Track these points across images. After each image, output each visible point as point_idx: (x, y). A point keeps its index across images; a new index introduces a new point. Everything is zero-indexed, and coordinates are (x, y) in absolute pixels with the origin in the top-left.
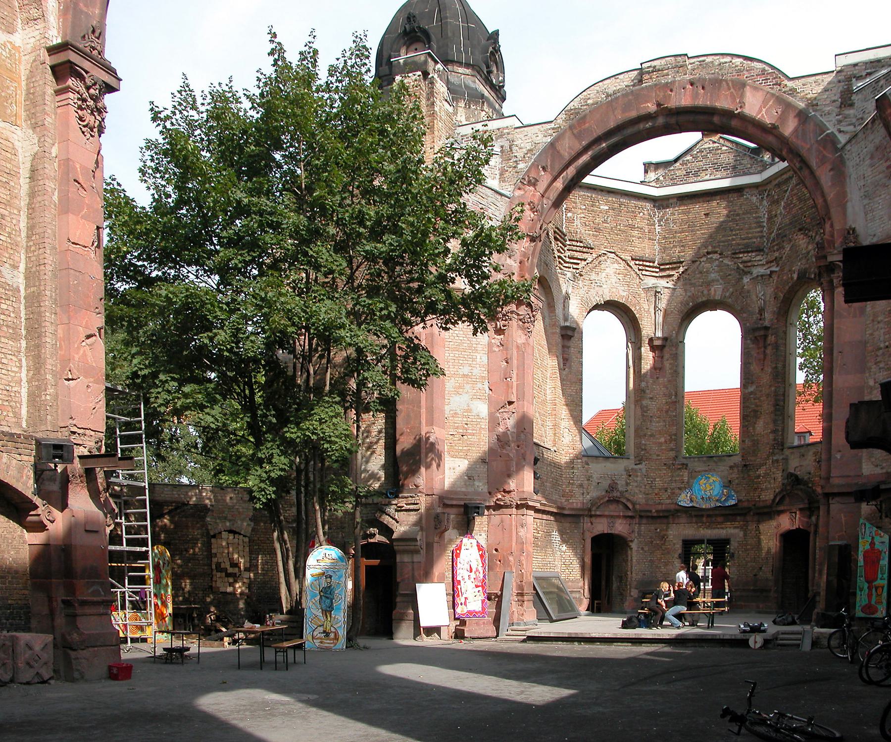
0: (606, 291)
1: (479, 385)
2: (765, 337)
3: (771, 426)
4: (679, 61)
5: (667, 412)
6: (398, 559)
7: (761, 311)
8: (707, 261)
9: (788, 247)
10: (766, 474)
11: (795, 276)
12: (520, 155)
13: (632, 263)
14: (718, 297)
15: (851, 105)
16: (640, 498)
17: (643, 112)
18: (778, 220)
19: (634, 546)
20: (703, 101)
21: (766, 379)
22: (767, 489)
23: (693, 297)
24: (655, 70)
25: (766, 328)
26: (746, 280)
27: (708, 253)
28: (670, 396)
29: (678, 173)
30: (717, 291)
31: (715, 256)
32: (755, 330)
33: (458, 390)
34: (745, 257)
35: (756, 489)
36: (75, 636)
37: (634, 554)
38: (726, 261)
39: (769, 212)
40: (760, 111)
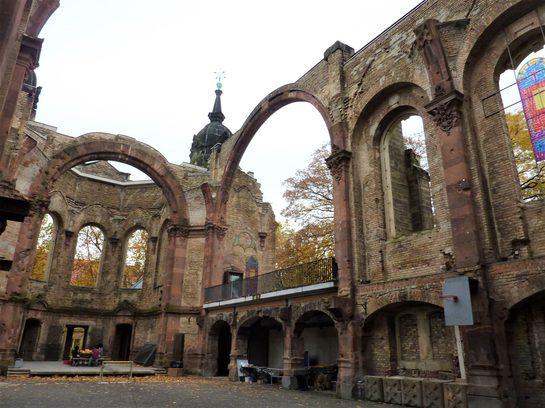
0: (54, 207)
1: (14, 238)
2: (116, 243)
3: (115, 279)
5: (68, 264)
7: (116, 232)
8: (96, 207)
9: (132, 212)
10: (110, 299)
11: (135, 224)
12: (57, 144)
13: (66, 198)
14: (98, 222)
15: (187, 179)
16: (49, 302)
18: (129, 201)
20: (139, 157)
22: (109, 305)
24: (123, 139)
25: (118, 240)
26: (111, 219)
27: (97, 204)
29: (89, 170)
30: (98, 220)
31: (100, 206)
32: (112, 239)
34: (112, 210)
35: (104, 304)
38: (104, 209)
39: (124, 197)
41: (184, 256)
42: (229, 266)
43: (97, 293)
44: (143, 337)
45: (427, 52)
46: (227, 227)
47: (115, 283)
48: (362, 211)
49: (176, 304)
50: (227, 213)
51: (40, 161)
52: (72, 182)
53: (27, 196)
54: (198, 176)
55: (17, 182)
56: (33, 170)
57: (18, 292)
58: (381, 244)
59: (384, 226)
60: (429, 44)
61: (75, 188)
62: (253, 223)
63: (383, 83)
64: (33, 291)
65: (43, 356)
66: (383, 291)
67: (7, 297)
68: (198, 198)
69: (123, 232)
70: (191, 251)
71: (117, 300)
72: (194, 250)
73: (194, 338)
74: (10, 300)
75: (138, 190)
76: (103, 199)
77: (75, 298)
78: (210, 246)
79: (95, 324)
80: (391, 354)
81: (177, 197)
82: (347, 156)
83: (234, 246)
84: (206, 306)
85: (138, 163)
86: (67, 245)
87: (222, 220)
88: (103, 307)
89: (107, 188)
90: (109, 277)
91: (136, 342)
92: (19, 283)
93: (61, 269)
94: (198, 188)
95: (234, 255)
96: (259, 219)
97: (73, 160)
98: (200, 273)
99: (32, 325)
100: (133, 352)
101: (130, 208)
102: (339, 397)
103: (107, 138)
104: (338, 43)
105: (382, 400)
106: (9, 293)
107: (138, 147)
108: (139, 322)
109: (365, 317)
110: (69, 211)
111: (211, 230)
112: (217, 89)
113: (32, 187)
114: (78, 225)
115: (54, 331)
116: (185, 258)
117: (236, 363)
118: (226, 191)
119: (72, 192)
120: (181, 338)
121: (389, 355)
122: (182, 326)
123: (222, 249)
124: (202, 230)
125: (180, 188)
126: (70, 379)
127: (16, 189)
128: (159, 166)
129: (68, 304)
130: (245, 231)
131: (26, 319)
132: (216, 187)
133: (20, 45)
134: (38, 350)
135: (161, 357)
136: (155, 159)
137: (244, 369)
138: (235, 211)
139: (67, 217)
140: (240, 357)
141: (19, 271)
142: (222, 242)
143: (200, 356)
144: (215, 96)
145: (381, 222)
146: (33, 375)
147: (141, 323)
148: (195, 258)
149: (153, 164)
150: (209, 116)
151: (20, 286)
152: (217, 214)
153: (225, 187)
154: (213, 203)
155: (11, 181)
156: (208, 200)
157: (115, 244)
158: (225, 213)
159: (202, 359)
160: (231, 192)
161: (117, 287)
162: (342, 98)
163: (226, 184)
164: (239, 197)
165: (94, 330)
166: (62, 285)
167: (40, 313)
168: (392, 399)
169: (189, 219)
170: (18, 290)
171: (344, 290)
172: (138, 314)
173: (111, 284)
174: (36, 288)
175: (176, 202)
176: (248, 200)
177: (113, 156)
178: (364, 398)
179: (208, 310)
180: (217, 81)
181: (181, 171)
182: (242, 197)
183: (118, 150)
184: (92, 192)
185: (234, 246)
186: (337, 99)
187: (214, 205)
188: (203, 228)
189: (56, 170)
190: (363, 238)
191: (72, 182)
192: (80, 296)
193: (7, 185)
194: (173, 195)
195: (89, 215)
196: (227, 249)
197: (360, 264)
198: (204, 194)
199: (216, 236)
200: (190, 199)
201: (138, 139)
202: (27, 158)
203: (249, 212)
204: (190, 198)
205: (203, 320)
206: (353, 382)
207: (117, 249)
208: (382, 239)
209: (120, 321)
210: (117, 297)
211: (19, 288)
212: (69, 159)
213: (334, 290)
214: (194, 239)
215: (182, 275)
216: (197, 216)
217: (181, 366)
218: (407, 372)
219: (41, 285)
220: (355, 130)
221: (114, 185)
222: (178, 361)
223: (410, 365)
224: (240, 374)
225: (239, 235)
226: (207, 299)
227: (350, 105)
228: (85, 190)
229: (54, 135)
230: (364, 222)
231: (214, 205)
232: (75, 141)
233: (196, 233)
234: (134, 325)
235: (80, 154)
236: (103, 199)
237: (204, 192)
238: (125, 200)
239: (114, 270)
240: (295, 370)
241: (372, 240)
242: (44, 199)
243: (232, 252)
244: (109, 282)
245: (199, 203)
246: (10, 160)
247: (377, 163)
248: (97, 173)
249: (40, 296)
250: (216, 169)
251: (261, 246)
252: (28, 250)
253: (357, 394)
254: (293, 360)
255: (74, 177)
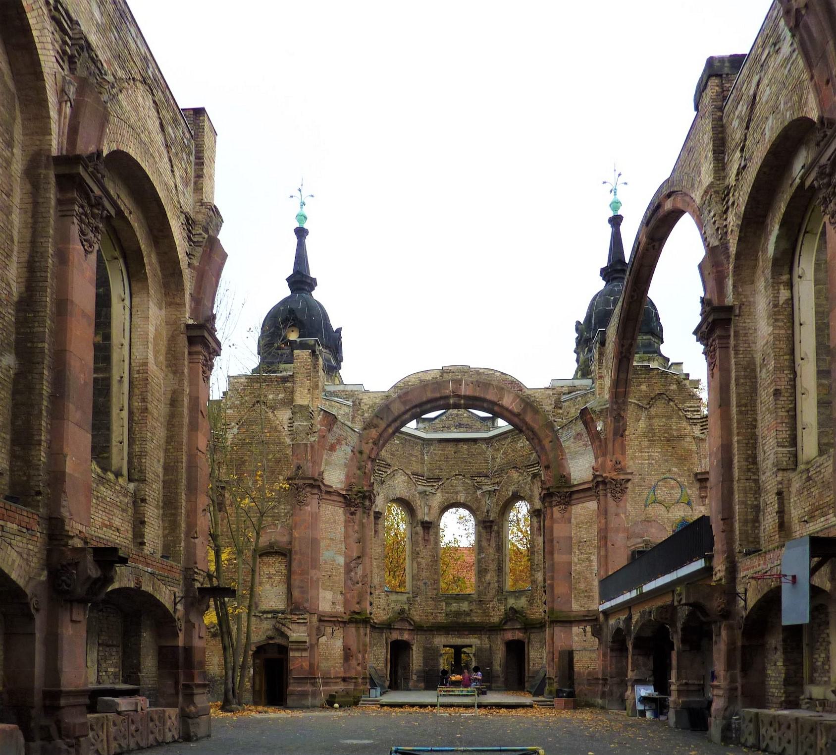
0: (398, 492)
1: (339, 546)
2: (491, 527)
3: (496, 578)
4: (465, 370)
6: (292, 654)
7: (488, 511)
10: (494, 607)
11: (510, 494)
12: (365, 408)
15: (560, 408)
16: (417, 618)
17: (443, 395)
18: (498, 460)
19: (414, 648)
21: (491, 551)
23: (447, 500)
25: (492, 522)
26: (479, 492)
28: (433, 557)
29: (438, 426)
30: (462, 498)
31: (461, 477)
32: (484, 522)
33: (327, 548)
34: (479, 479)
36: (192, 708)
37: (414, 653)
40: (511, 404)
41: (567, 534)
42: (639, 540)
43: (475, 601)
44: (539, 657)
45: (805, 36)
46: (630, 477)
47: (496, 585)
48: (755, 420)
49: (565, 608)
50: (629, 452)
51: (349, 438)
52: (416, 451)
53: (342, 489)
54: (576, 398)
55: (325, 475)
56: (343, 454)
57: (357, 610)
58: (779, 478)
59: (793, 440)
60: (805, 17)
61: (423, 459)
62: (683, 459)
63: (769, 130)
64: (393, 605)
65: (422, 685)
66: (764, 567)
67: (346, 618)
68: (578, 436)
69: (497, 510)
70: (578, 524)
71: (502, 608)
72: (583, 523)
73: (594, 656)
74: (351, 621)
75: (509, 440)
76: (463, 466)
77: (448, 609)
78: (603, 512)
79: (479, 642)
80: (786, 673)
81: (546, 442)
82: (723, 316)
83: (646, 506)
84: (602, 608)
85: (478, 403)
86: (426, 541)
87: (619, 467)
88: (486, 619)
89: (466, 447)
90: (488, 577)
91: (531, 664)
92: (356, 600)
93: (424, 574)
94: (576, 419)
95: (648, 521)
96: (694, 448)
97: (389, 426)
98: (594, 558)
99: (399, 650)
100: (529, 677)
101: (501, 470)
102: (710, 741)
103: (429, 377)
104: (711, 62)
105: (756, 747)
106: (348, 612)
107: (475, 378)
108: (532, 636)
109: (744, 614)
110: (420, 493)
111: (601, 487)
112: (611, 214)
113: (347, 477)
114: (435, 511)
115: (431, 654)
116: (571, 538)
117: (633, 690)
118: (619, 414)
119: (420, 466)
120: (569, 656)
121: (783, 675)
122: (576, 638)
123: (623, 516)
124: (589, 489)
125: (550, 425)
126: (422, 710)
127: (326, 483)
128: (511, 398)
129: (441, 619)
130: (667, 475)
131: (389, 641)
132: (601, 411)
133: (186, 339)
134: (415, 677)
135: (550, 684)
136: (503, 389)
137: (644, 700)
138: (645, 443)
139: (418, 502)
140: (641, 682)
141: (354, 584)
142: (622, 504)
143: (601, 682)
144: (608, 230)
145: (785, 435)
146: (382, 706)
147: (535, 638)
148: (585, 536)
149: (502, 398)
150: (601, 275)
151: (358, 603)
152: (608, 457)
153: (615, 407)
154: (600, 441)
155: (316, 476)
156: (595, 437)
157: (490, 527)
158: (623, 452)
159: (604, 685)
160: (630, 413)
161: (501, 590)
162: (717, 192)
163: (617, 403)
164: (650, 418)
165: (480, 650)
166: (430, 594)
167: (406, 632)
168: (767, 745)
169: (570, 474)
170: (357, 608)
171: (720, 568)
172: (532, 626)
173: (492, 586)
174: (396, 602)
175: (546, 452)
176: (669, 417)
177: (429, 406)
178: (739, 744)
179: (606, 613)
180: (611, 198)
181: (549, 396)
182: (657, 416)
183: (447, 392)
184: (446, 459)
185: (646, 506)
186: (708, 197)
187: (603, 441)
188: (590, 485)
189: (370, 445)
190: (756, 473)
191: (416, 451)
192: (455, 606)
193: (311, 482)
194: (540, 441)
195: (447, 493)
196: (633, 513)
197: (745, 522)
198: (587, 428)
199: (609, 495)
200: (567, 440)
201: (473, 365)
202: (331, 439)
203: (671, 440)
204: (567, 440)
205: (601, 629)
206: (724, 718)
207: (493, 534)
208: (783, 470)
209: (509, 636)
210: (501, 603)
211: (357, 606)
212: (383, 425)
213: (708, 571)
214: (580, 505)
215: (570, 564)
216: (581, 467)
217: (571, 695)
218: (812, 703)
219: (404, 598)
220: (738, 255)
221: (475, 440)
222: (568, 688)
223: (816, 692)
224: (640, 707)
225: (656, 485)
226: (605, 596)
227: (730, 202)
228: (437, 458)
229: (360, 397)
230: (760, 440)
231: (603, 441)
232: (387, 396)
233: (582, 495)
234: (526, 641)
235: (396, 414)
236: (463, 466)
237: (586, 424)
238: (494, 459)
239: (493, 566)
240: (685, 699)
241: (768, 474)
242: (365, 488)
243: (643, 517)
244: (489, 583)
245: (581, 443)
246: (309, 449)
247: (785, 314)
248: (449, 428)
249: (402, 611)
250: (600, 377)
251: (702, 497)
252: (359, 557)
253: (729, 735)
254: (681, 685)
255: (417, 444)
